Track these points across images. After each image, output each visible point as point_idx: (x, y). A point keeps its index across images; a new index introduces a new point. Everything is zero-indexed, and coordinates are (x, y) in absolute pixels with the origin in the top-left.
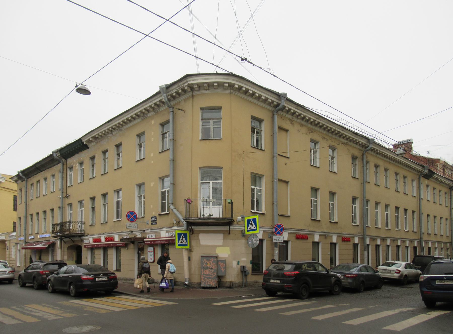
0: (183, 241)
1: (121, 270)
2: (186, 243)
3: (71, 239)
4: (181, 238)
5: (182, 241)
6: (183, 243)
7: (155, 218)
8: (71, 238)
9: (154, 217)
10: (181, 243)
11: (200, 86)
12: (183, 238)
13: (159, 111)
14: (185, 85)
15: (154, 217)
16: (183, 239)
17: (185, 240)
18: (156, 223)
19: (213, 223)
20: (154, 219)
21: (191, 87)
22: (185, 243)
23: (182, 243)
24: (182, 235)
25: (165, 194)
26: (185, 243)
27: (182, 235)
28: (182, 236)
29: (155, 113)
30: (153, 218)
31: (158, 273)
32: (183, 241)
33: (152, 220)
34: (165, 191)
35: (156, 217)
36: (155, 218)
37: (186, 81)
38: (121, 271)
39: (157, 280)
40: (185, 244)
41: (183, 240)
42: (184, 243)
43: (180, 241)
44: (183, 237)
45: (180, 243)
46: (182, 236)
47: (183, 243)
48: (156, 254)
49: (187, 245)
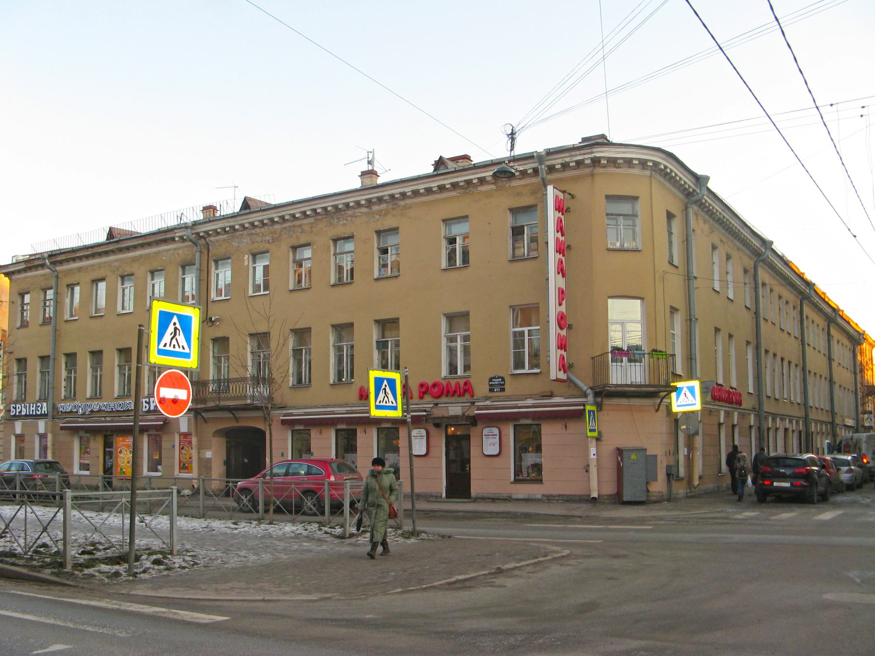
0: (174, 342)
1: (542, 480)
2: (187, 350)
3: (234, 415)
4: (171, 328)
5: (172, 339)
6: (174, 347)
7: (501, 380)
8: (234, 412)
9: (499, 378)
10: (168, 348)
11: (613, 162)
12: (176, 329)
13: (507, 185)
14: (587, 157)
15: (499, 378)
16: (175, 334)
17: (181, 338)
18: (503, 390)
19: (634, 392)
20: (496, 382)
21: (596, 162)
22: (183, 348)
23: (171, 349)
24: (175, 319)
25: (524, 336)
26: (183, 348)
27: (175, 319)
28: (175, 324)
29: (497, 187)
30: (494, 380)
31: (509, 482)
32: (174, 342)
33: (491, 383)
34: (522, 333)
35: (503, 380)
36: (501, 380)
37: (589, 151)
38: (542, 483)
39: (509, 495)
40: (181, 350)
41: (177, 336)
42: (177, 349)
43: (167, 338)
44: (178, 326)
45: (380, 402)
46: (175, 324)
47: (174, 347)
48: (430, 438)
49: (187, 356)
